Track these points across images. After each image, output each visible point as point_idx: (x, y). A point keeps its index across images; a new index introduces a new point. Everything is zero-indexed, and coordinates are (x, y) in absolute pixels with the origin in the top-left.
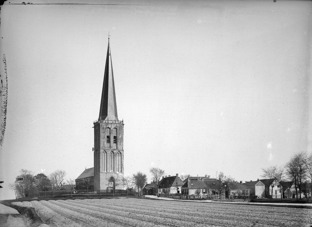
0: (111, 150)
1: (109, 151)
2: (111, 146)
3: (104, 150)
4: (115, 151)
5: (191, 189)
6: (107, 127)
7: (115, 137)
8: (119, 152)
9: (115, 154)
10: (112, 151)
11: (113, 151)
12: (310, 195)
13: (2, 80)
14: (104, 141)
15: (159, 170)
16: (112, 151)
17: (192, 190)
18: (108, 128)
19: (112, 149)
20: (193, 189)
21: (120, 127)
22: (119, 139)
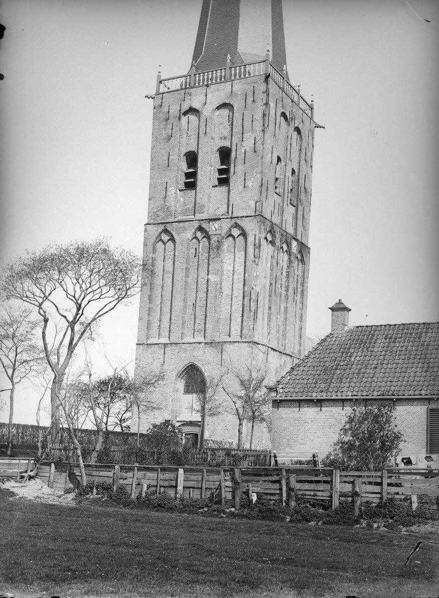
0: (196, 225)
1: (184, 229)
2: (198, 200)
3: (162, 227)
4: (213, 228)
5: (300, 403)
6: (185, 107)
7: (225, 154)
8: (237, 226)
9: (214, 239)
10: (200, 229)
11: (204, 225)
12: (327, 596)
13: (323, 128)
14: (167, 180)
15: (73, 251)
16: (200, 229)
17: (310, 412)
18: (192, 110)
19: (205, 216)
20: (319, 403)
21: (250, 94)
22: (240, 157)
